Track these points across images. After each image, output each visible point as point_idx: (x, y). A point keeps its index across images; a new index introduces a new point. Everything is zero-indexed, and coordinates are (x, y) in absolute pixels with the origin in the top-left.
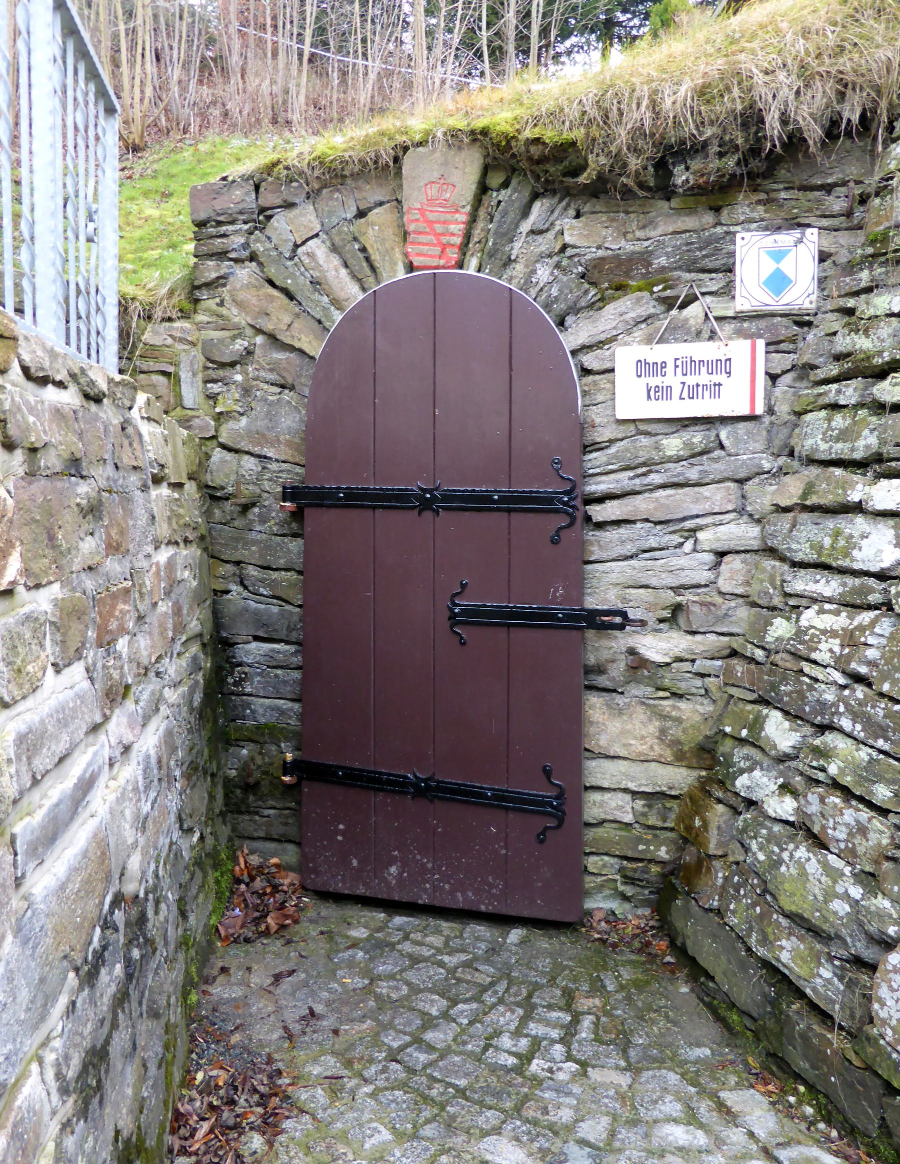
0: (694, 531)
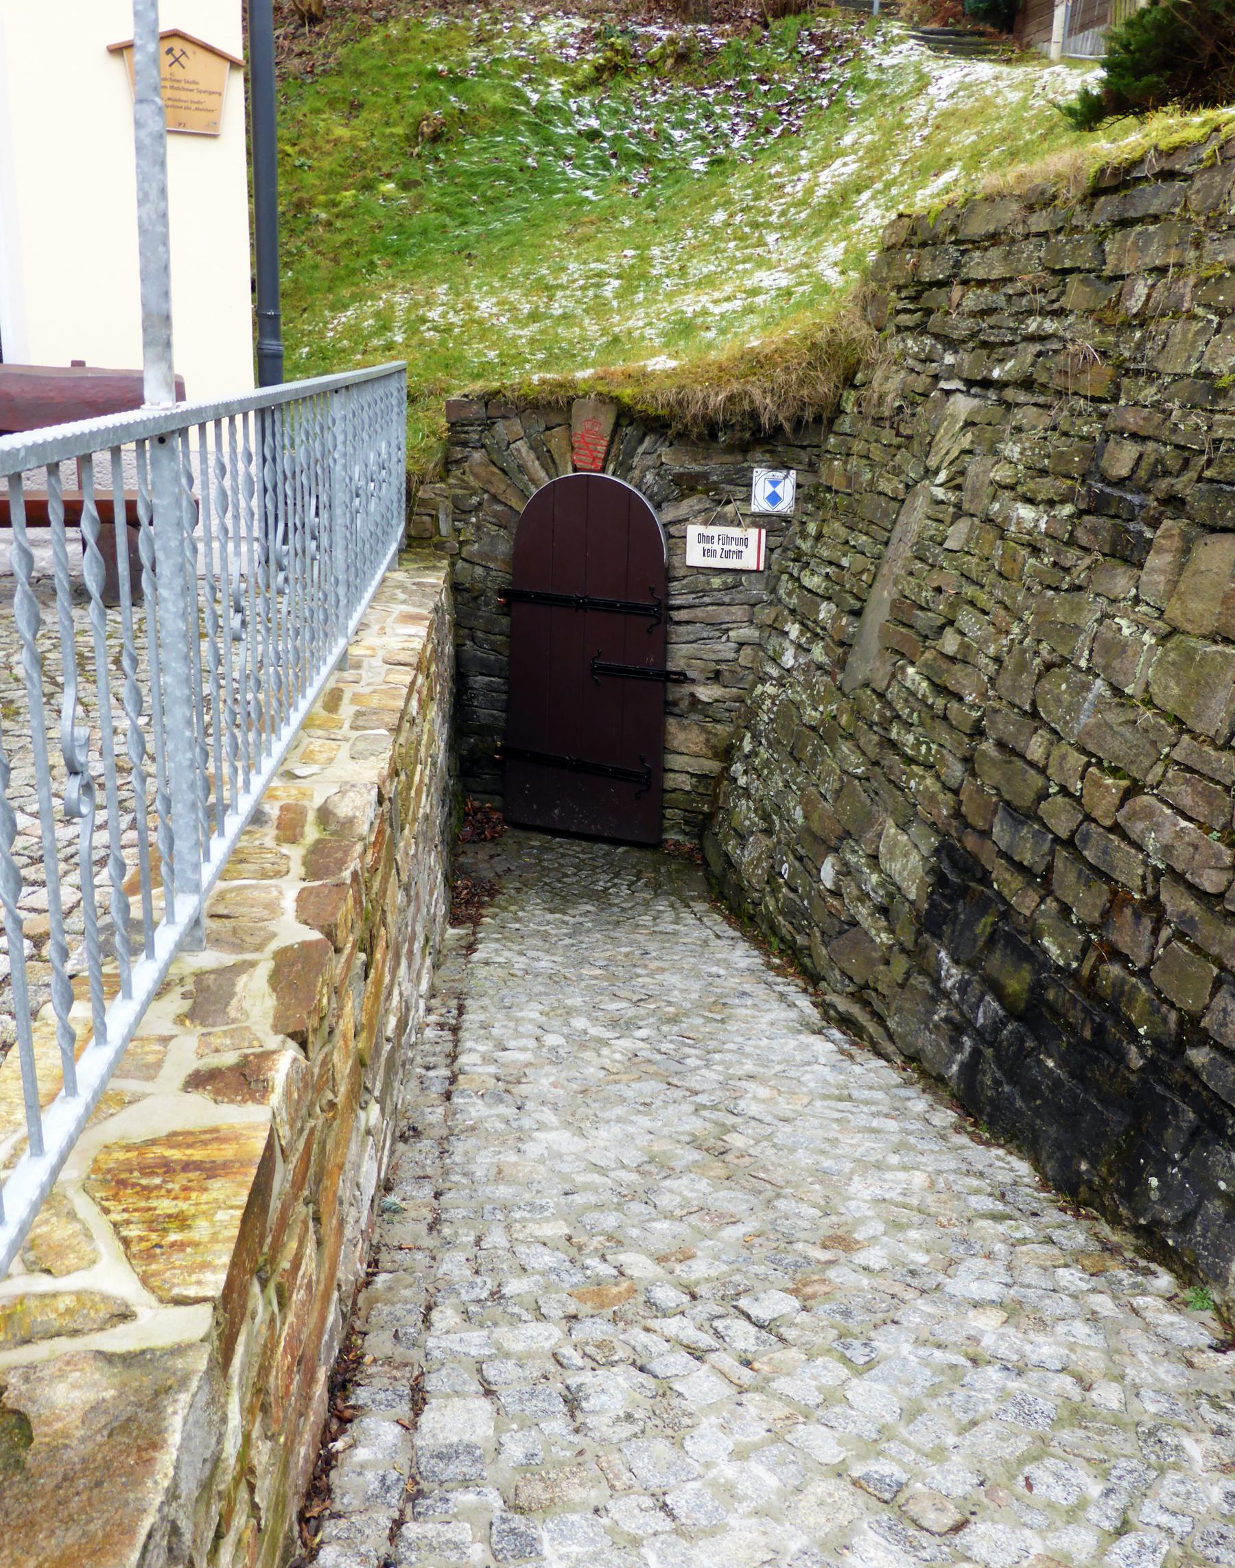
0: (728, 630)
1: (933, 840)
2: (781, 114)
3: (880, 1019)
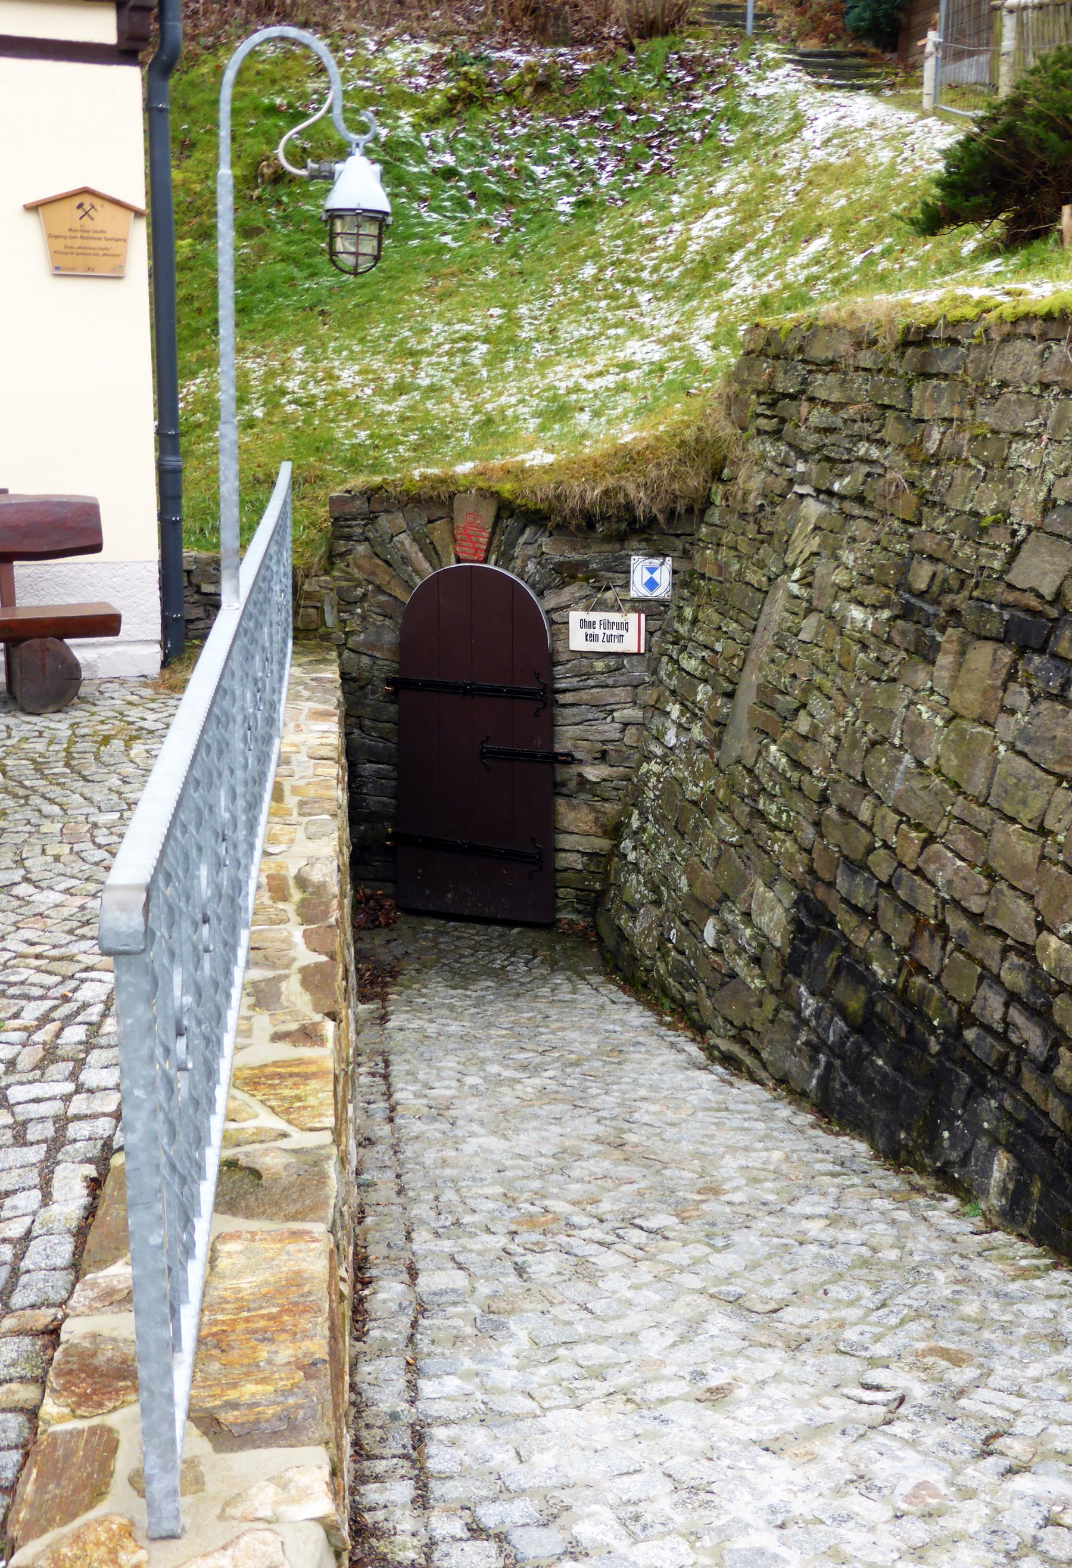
0: (612, 711)
1: (793, 894)
2: (651, 147)
3: (755, 1052)
